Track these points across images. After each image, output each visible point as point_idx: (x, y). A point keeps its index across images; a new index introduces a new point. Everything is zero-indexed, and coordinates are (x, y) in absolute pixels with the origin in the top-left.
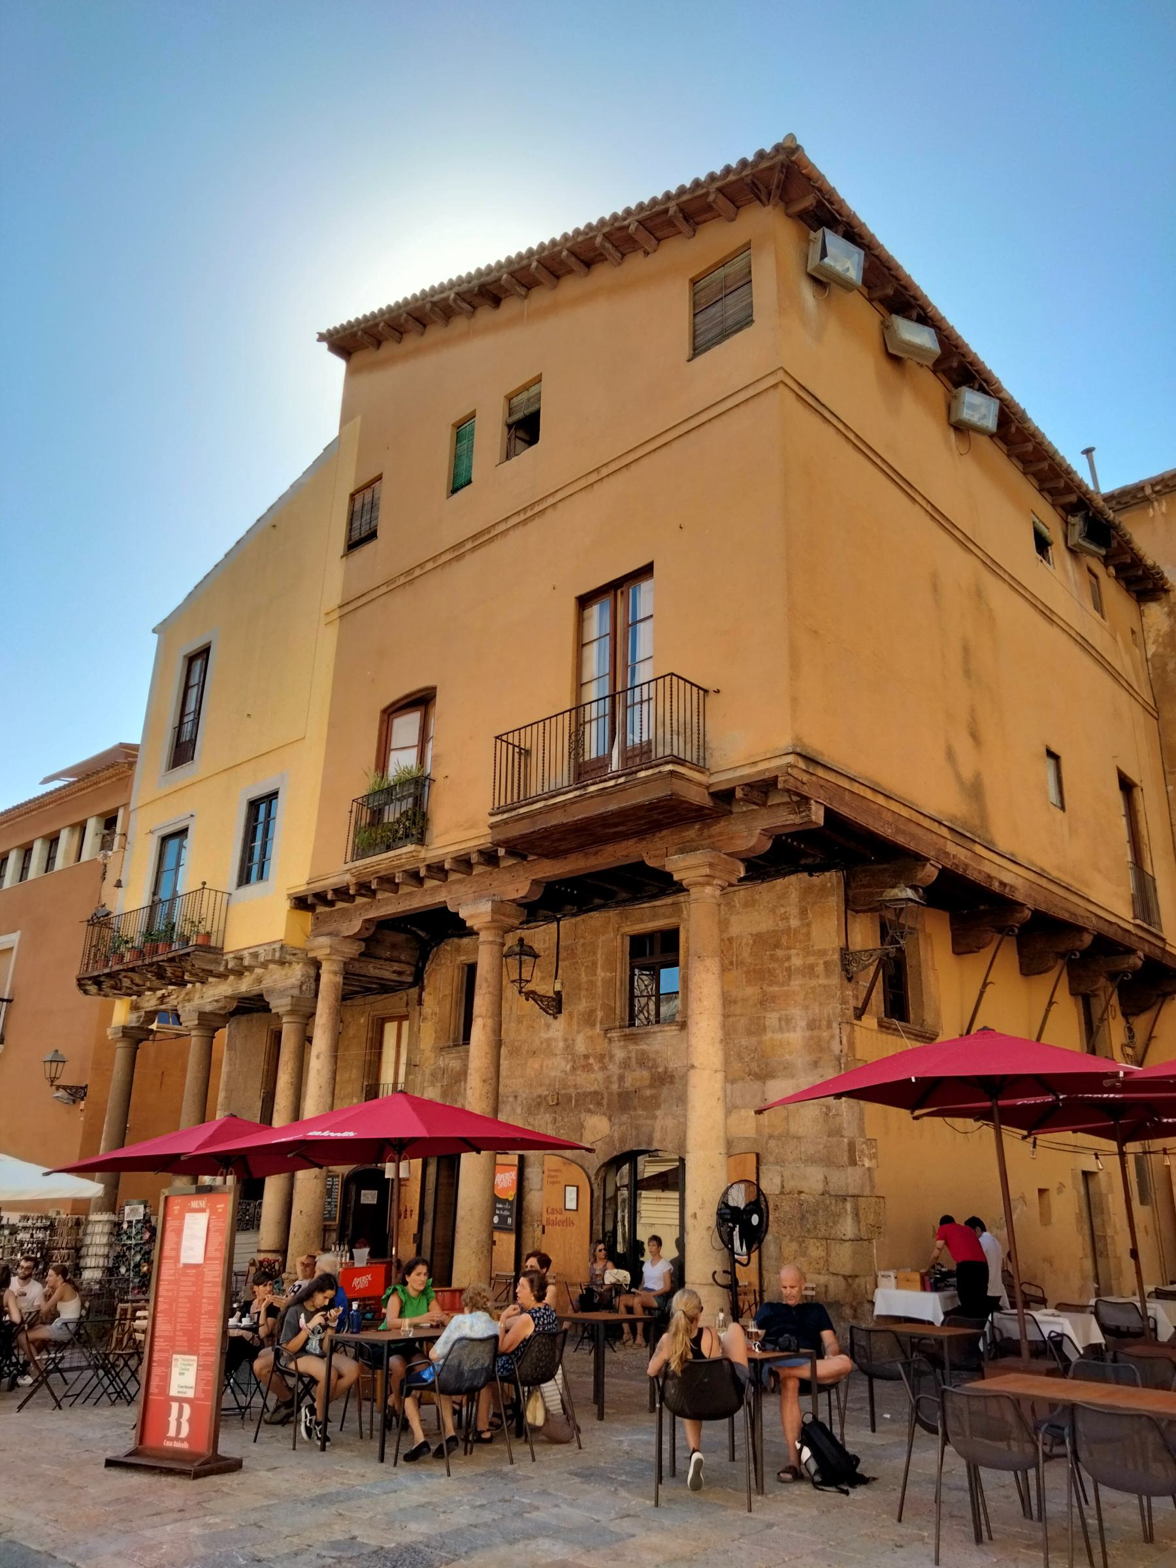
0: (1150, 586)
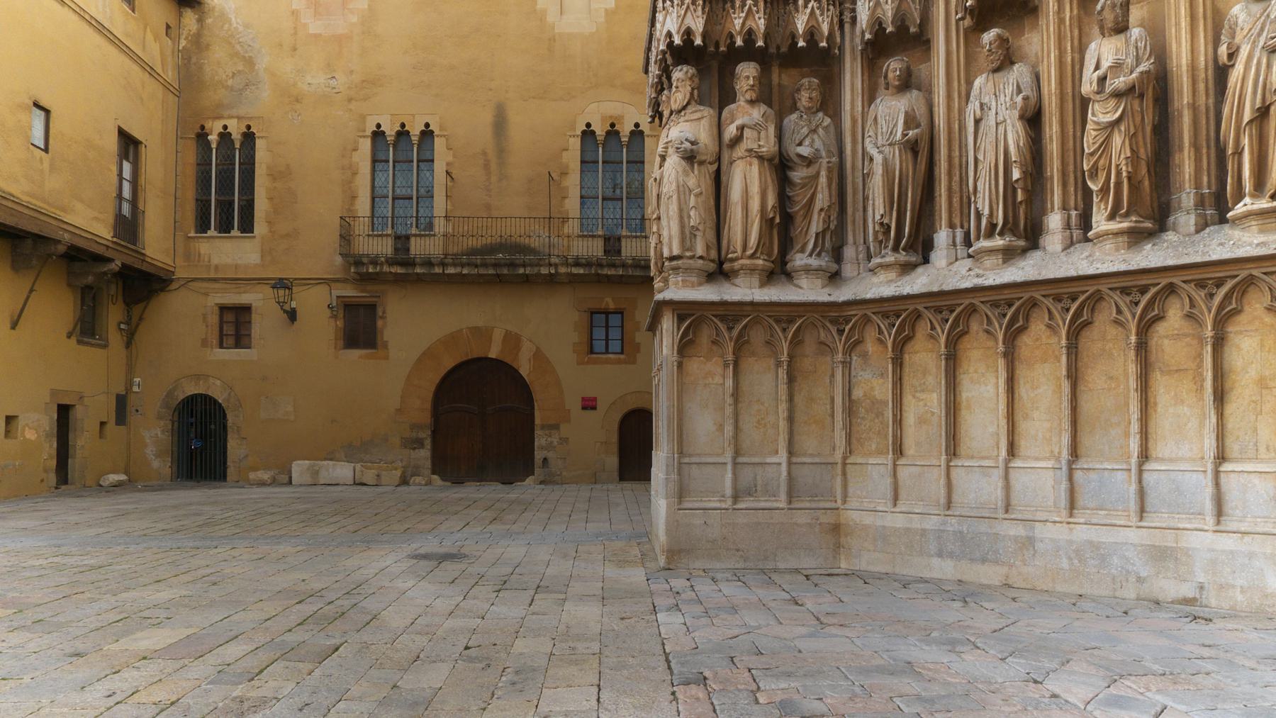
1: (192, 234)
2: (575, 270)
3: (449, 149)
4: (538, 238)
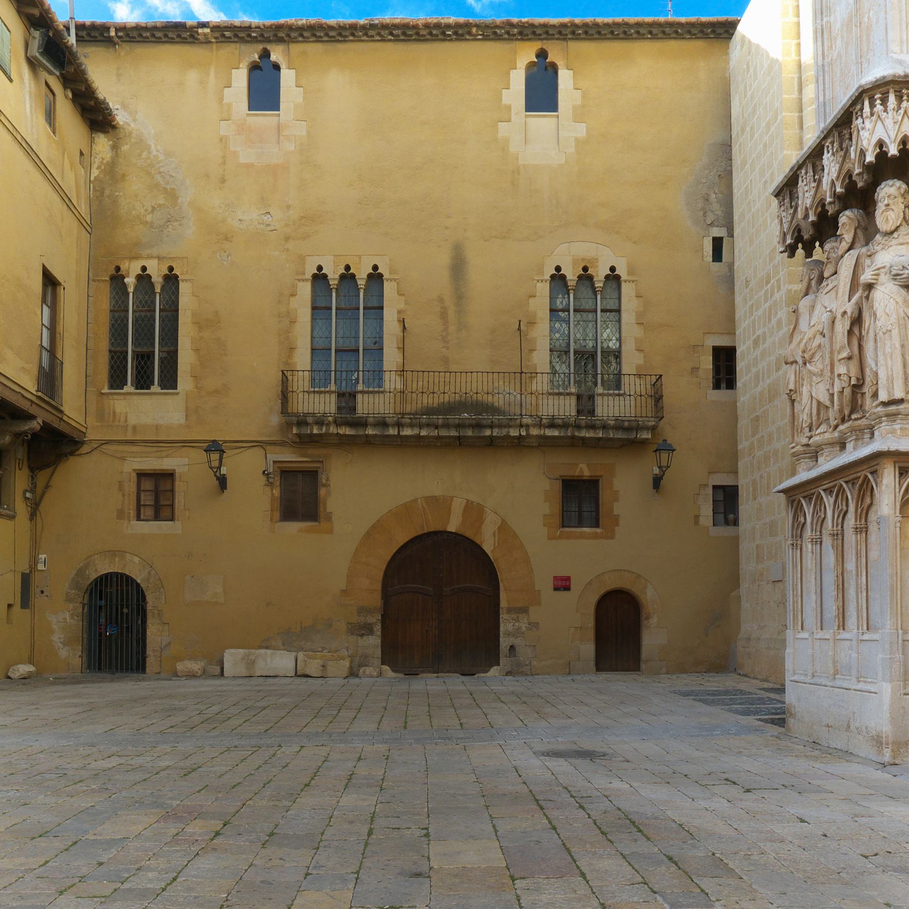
0: (101, 118)
1: (106, 390)
2: (549, 432)
3: (400, 294)
4: (505, 395)
